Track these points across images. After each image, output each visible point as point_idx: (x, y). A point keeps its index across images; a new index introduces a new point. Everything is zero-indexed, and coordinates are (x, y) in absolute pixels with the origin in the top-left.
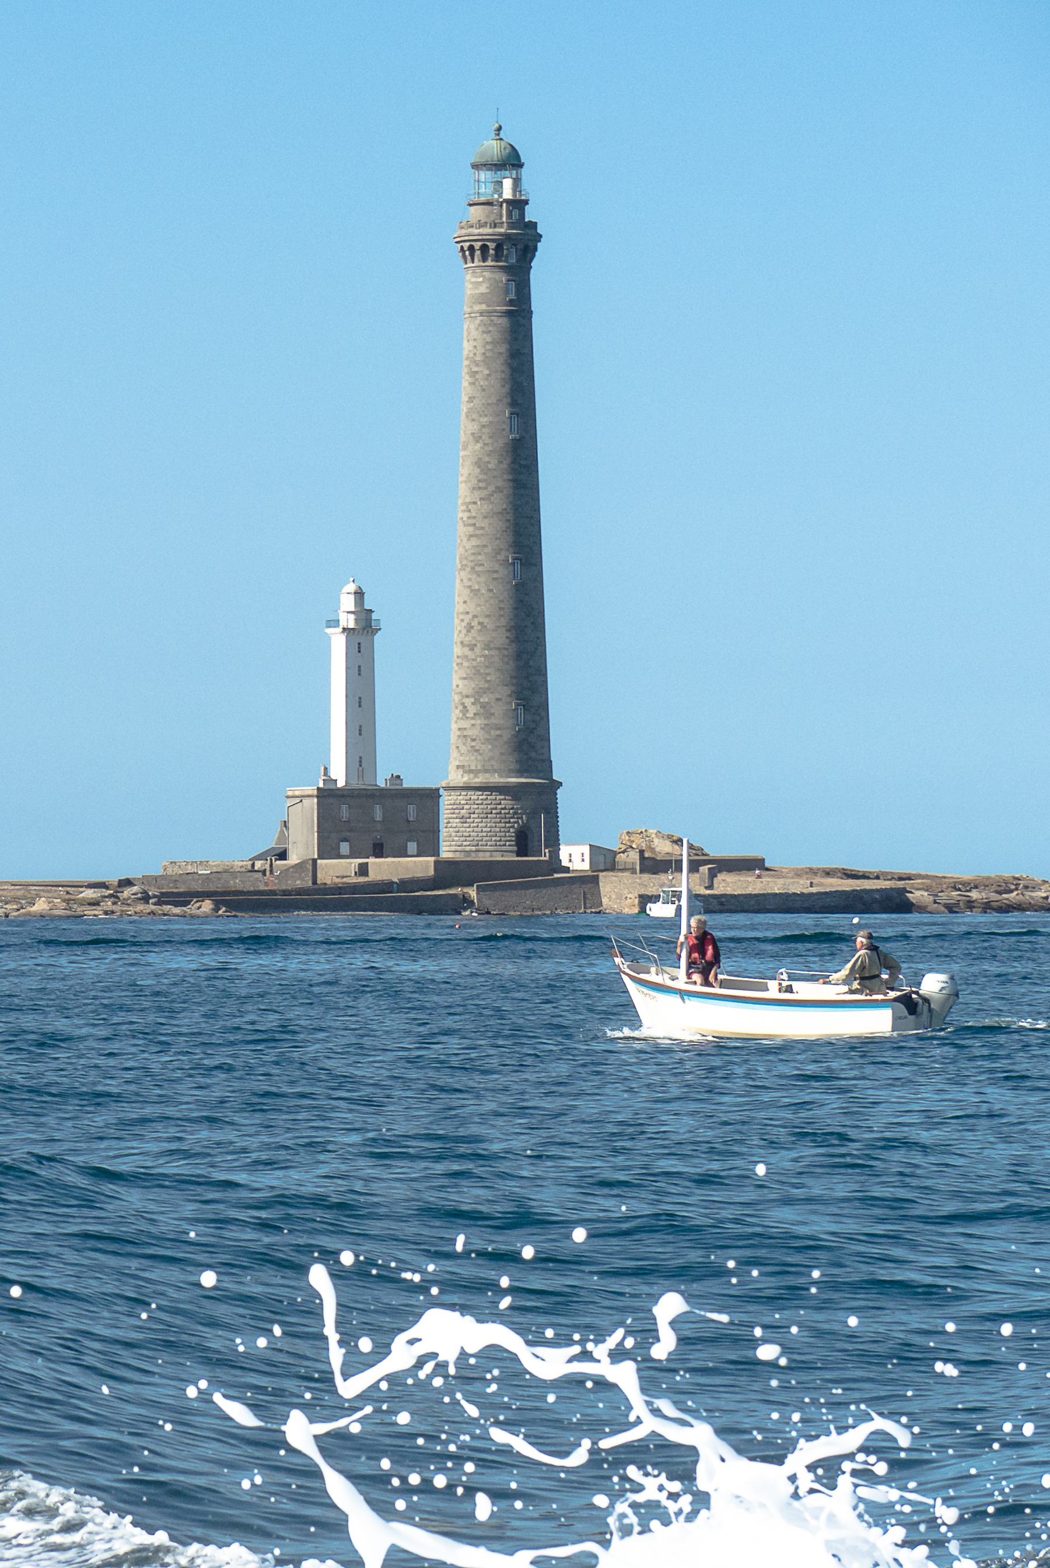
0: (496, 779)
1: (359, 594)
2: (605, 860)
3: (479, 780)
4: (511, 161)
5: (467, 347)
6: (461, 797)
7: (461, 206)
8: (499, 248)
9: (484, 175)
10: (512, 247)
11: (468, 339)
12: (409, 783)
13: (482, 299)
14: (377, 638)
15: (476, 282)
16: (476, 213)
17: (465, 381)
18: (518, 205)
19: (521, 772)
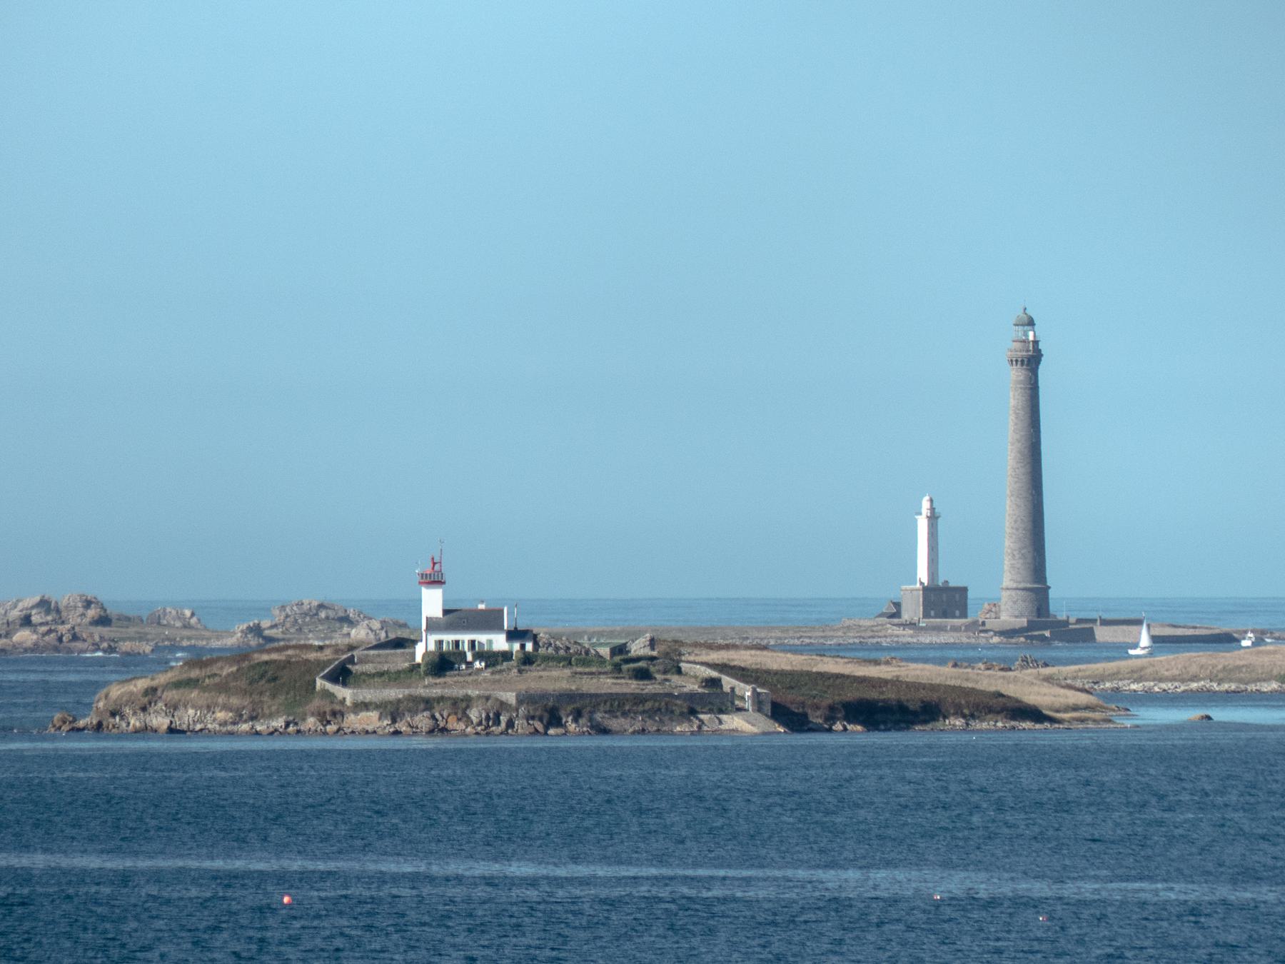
0: (1029, 585)
1: (931, 501)
2: (701, 720)
3: (1022, 586)
4: (1031, 323)
5: (1012, 402)
6: (1008, 592)
7: (1006, 341)
8: (1029, 360)
9: (1021, 328)
10: (1031, 360)
11: (1013, 399)
12: (952, 584)
13: (1020, 382)
14: (940, 520)
15: (1015, 375)
16: (1018, 345)
17: (1012, 417)
18: (1036, 342)
19: (1035, 582)
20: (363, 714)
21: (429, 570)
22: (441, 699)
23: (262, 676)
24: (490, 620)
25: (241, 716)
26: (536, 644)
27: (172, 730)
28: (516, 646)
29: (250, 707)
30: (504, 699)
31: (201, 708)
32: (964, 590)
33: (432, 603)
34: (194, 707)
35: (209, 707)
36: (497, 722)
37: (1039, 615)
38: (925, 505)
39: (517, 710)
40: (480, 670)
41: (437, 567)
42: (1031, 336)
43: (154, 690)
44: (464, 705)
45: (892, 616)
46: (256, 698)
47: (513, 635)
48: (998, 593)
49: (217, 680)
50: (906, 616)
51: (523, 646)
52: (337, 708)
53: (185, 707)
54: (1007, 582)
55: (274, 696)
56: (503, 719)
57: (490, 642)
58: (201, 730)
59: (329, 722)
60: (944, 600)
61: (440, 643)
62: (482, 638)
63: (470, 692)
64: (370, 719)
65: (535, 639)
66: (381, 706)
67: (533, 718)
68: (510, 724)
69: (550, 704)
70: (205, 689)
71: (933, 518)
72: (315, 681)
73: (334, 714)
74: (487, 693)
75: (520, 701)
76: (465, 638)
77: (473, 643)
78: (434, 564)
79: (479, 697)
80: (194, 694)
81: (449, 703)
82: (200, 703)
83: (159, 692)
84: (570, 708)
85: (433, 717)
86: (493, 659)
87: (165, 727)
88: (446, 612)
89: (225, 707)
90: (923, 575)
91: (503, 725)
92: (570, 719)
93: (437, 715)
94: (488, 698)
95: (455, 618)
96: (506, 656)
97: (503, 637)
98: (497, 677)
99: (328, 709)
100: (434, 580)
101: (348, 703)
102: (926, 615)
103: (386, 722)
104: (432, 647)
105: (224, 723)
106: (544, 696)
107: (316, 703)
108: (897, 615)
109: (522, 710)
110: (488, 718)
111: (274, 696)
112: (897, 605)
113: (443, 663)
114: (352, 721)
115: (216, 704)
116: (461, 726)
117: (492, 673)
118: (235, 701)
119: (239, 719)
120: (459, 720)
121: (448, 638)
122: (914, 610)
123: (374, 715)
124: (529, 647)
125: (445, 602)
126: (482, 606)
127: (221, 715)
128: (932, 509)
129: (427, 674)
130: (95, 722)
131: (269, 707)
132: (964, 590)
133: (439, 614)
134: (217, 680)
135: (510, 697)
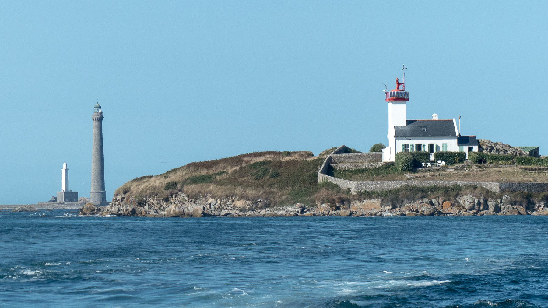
4: (100, 107)
5: (94, 132)
7: (92, 113)
10: (100, 119)
15: (95, 123)
16: (96, 114)
18: (102, 113)
20: (367, 202)
21: (394, 88)
22: (434, 189)
23: (265, 173)
24: (444, 129)
25: (257, 203)
26: (480, 148)
27: (205, 215)
28: (466, 149)
29: (264, 196)
30: (488, 188)
31: (220, 198)
32: (77, 193)
33: (398, 115)
34: (213, 197)
35: (227, 197)
36: (486, 207)
37: (103, 200)
38: (64, 166)
39: (501, 197)
40: (444, 168)
41: (401, 87)
42: (100, 112)
43: (174, 184)
44: (455, 193)
45: (54, 201)
46: (267, 189)
47: (462, 140)
48: (88, 193)
49: (225, 176)
50: (58, 201)
51: (470, 149)
52: (345, 196)
53: (205, 197)
54: (92, 190)
55: (281, 188)
56: (491, 204)
57: (445, 145)
58: (226, 215)
59: (338, 208)
60: (71, 196)
61: (406, 146)
62: (439, 143)
63: (459, 183)
64: (372, 206)
65: (478, 143)
66: (383, 195)
67: (515, 203)
68: (497, 209)
69: (526, 192)
70: (220, 183)
71: (67, 170)
72: (317, 176)
73: (342, 201)
74: (474, 183)
75: (502, 191)
76: (426, 142)
77: (432, 146)
78: (399, 84)
79: (467, 187)
80: (212, 187)
81: (441, 192)
82: (219, 193)
83: (179, 187)
84: (541, 195)
85: (431, 203)
86: (451, 158)
87: (200, 212)
88: (409, 122)
89: (242, 197)
90: (64, 188)
91: (491, 209)
92: (542, 204)
93: (434, 201)
94: (475, 187)
95: (415, 128)
96: (461, 157)
97: (455, 141)
98: (459, 172)
99: (336, 198)
100: (399, 97)
101: (353, 192)
102: (65, 200)
103: (387, 208)
104: (400, 150)
105: (243, 210)
106: (520, 185)
107: (323, 193)
108: (56, 201)
109: (505, 197)
110: (479, 204)
111: (281, 188)
112: (55, 198)
113: (414, 162)
114: (358, 207)
115: (235, 195)
116: (455, 210)
117: (456, 169)
118: (250, 192)
119: (255, 206)
120: (453, 205)
121: (413, 142)
122: (61, 199)
123: (377, 202)
124: (475, 149)
125: (407, 118)
126: (435, 117)
127: (240, 203)
128: (67, 167)
129: (404, 170)
130: (130, 209)
131: (280, 197)
132: (77, 193)
133: (404, 124)
134: (225, 176)
135: (495, 187)
